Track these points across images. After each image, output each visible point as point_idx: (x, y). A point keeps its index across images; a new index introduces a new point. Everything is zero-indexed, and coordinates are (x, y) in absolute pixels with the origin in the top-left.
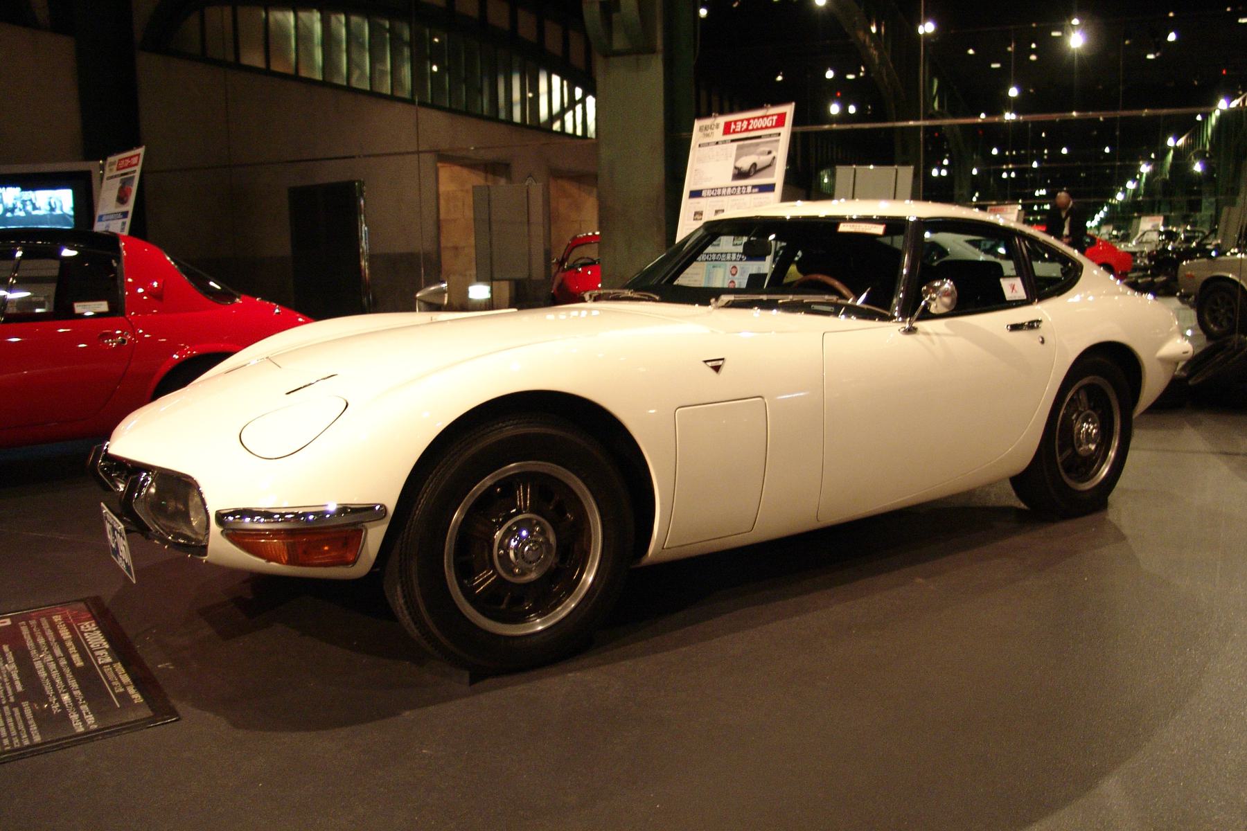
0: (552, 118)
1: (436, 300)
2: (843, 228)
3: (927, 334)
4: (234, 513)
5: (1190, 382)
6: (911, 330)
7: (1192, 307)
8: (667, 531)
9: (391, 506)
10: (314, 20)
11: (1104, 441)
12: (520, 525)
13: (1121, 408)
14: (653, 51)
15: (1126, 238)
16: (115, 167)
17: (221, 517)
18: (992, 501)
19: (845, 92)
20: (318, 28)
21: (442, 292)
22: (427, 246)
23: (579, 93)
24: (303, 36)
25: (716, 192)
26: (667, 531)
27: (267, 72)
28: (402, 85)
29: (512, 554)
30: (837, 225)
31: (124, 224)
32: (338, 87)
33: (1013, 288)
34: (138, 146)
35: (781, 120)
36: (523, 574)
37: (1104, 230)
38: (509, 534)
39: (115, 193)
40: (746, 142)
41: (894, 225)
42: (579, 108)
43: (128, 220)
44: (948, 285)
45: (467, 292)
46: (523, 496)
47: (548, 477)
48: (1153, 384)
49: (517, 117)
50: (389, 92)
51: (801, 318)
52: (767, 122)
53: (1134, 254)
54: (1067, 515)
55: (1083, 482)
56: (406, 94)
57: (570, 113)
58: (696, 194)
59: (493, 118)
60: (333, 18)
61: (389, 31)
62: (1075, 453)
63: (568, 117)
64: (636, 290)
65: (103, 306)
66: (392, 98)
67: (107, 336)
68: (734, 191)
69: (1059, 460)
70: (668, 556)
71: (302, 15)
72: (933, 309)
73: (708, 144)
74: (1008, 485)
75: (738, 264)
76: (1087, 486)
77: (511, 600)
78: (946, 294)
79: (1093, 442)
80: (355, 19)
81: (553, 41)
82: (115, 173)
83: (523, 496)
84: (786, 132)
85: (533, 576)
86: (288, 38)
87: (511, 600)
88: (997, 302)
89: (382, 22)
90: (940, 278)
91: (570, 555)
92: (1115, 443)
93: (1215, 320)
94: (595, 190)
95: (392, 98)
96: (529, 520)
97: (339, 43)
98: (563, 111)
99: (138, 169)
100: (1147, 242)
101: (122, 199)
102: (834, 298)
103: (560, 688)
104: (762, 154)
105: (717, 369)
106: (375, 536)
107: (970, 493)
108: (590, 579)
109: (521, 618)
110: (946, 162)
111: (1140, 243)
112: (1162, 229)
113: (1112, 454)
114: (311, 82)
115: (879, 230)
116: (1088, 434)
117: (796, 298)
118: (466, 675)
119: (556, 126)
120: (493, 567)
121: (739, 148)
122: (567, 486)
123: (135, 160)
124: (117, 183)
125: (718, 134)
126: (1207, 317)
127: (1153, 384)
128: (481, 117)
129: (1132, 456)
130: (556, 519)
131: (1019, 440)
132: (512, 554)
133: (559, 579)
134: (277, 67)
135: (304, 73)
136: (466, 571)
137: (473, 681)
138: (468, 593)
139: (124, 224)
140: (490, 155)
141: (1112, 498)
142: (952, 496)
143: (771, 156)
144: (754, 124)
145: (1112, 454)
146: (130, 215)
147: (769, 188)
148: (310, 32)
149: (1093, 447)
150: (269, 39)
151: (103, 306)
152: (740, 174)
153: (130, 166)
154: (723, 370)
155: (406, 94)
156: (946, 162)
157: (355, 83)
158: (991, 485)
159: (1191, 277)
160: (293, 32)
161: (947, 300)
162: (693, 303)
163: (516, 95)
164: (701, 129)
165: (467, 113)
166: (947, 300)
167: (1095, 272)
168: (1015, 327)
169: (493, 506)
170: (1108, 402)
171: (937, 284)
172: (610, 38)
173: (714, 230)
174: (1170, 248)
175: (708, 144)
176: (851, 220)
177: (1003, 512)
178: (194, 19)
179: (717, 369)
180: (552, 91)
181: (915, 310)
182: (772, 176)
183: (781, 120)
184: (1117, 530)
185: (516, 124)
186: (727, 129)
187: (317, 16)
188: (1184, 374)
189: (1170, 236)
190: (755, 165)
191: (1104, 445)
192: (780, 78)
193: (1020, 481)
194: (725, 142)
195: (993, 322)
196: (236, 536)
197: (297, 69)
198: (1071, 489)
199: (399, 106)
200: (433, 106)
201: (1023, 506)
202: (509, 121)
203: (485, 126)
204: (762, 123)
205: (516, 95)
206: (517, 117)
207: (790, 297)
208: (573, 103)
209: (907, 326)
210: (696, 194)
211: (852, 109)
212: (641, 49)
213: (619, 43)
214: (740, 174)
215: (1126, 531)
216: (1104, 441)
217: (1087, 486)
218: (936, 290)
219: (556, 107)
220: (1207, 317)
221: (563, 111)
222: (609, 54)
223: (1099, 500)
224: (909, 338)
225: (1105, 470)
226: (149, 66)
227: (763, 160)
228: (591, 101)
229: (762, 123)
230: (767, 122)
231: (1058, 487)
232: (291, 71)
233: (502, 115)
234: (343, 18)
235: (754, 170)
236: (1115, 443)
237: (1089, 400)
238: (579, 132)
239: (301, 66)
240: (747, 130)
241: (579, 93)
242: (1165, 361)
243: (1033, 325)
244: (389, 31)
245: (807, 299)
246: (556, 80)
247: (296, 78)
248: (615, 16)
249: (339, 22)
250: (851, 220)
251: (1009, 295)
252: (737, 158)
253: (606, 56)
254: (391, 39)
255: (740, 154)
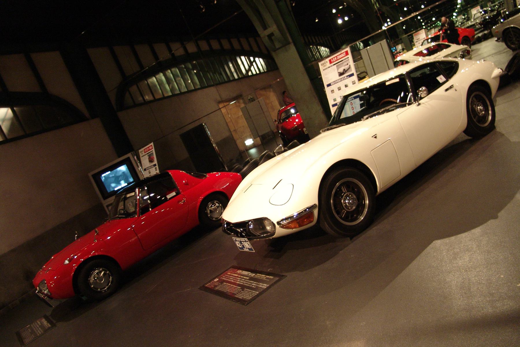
0: (247, 72)
1: (279, 151)
2: (387, 84)
3: (423, 103)
4: (282, 220)
5: (509, 74)
6: (419, 104)
7: (502, 42)
8: (381, 183)
9: (317, 203)
10: (161, 76)
11: (486, 109)
12: (347, 196)
13: (487, 97)
14: (289, 43)
15: (468, 19)
16: (143, 152)
17: (278, 223)
18: (461, 140)
19: (341, 14)
20: (163, 78)
21: (281, 147)
22: (227, 134)
23: (252, 59)
24: (160, 83)
25: (335, 82)
26: (381, 183)
27: (155, 100)
28: (196, 84)
29: (347, 204)
30: (385, 83)
31: (156, 168)
32: (178, 95)
33: (441, 79)
34: (151, 143)
35: (347, 53)
36: (351, 208)
37: (459, 18)
38: (345, 200)
39: (147, 160)
40: (338, 64)
41: (400, 76)
42: (254, 64)
43: (157, 167)
44: (424, 88)
45: (245, 144)
46: (344, 190)
47: (348, 182)
48: (494, 86)
49: (236, 77)
50: (193, 88)
51: (386, 115)
52: (343, 55)
53: (474, 25)
54: (484, 135)
55: (486, 123)
56: (199, 87)
57: (252, 67)
58: (329, 85)
59: (229, 81)
60: (167, 73)
61: (185, 68)
62: (479, 117)
63: (252, 68)
64: (337, 124)
65: (174, 194)
66: (196, 90)
67: (179, 202)
68: (341, 80)
69: (475, 120)
70: (383, 190)
71: (157, 76)
72: (422, 96)
73: (326, 69)
74: (464, 134)
75: (352, 101)
76: (487, 124)
77: (352, 215)
78: (424, 90)
79: (483, 111)
80: (173, 69)
81: (236, 46)
82: (144, 154)
83: (344, 190)
84: (350, 56)
85: (354, 208)
86: (155, 86)
87: (352, 215)
88: (439, 85)
89: (181, 66)
90: (421, 87)
91: (360, 198)
92: (490, 108)
93: (513, 43)
94: (271, 90)
95: (196, 90)
96: (347, 195)
97: (172, 80)
98: (250, 67)
99: (153, 150)
100: (477, 18)
101: (151, 161)
102: (394, 105)
103: (373, 231)
104: (345, 65)
105: (376, 137)
106: (316, 212)
107: (453, 141)
108: (368, 202)
109: (356, 219)
110: (388, 20)
111: (475, 19)
112: (481, 11)
113: (490, 112)
114: (169, 97)
115: (397, 80)
116: (480, 109)
117: (384, 109)
118: (349, 238)
119: (250, 74)
120: (344, 209)
121: (337, 66)
122: (353, 183)
123: (151, 148)
124: (147, 157)
125: (328, 64)
126: (509, 44)
127: (494, 86)
128: (225, 82)
129: (496, 109)
130: (353, 191)
131: (460, 120)
132: (347, 204)
133: (360, 206)
134: (157, 97)
135: (166, 95)
136: (338, 213)
137: (351, 239)
138: (341, 218)
139: (156, 168)
140: (235, 95)
141: (496, 124)
142: (449, 143)
143: (348, 66)
144: (339, 57)
145: (490, 112)
146: (157, 164)
147: (352, 75)
148: (162, 81)
149: (483, 112)
150: (151, 89)
151: (174, 194)
152: (341, 74)
153: (149, 150)
154: (377, 137)
155: (199, 87)
156: (388, 20)
157: (183, 91)
158: (459, 135)
159: (497, 32)
160: (157, 83)
161: (425, 92)
162: (353, 122)
163: (233, 70)
164: (322, 65)
165: (220, 84)
166: (425, 92)
167: (463, 71)
168: (447, 90)
169: (338, 195)
170: (483, 98)
171: (421, 89)
172: (274, 46)
173: (346, 98)
174: (487, 18)
175: (326, 69)
176: (388, 81)
177: (465, 142)
178: (127, 95)
179: (376, 137)
180: (243, 62)
181: (417, 98)
182: (351, 71)
183: (347, 53)
184: (500, 133)
185: (237, 79)
186: (330, 62)
187: (161, 74)
188: (506, 72)
189: (486, 12)
190: (344, 70)
191: (486, 110)
192: (317, 21)
193: (466, 131)
194: (331, 66)
195: (440, 91)
196: (283, 227)
197: (163, 95)
198: (483, 127)
199: (199, 92)
200: (209, 86)
201: (470, 138)
202: (235, 80)
203: (229, 85)
204: (341, 56)
205: (233, 70)
206: (236, 77)
207: (383, 109)
208: (251, 63)
209: (417, 104)
210: (329, 85)
211: (346, 19)
212: (285, 44)
213: (277, 45)
214: (341, 74)
215: (504, 132)
216: (486, 109)
217: (487, 124)
218: (421, 91)
219: (247, 67)
220: (509, 44)
221: (250, 67)
222: (275, 50)
223: (492, 126)
224: (420, 107)
225: (490, 118)
226: (121, 115)
227: (346, 67)
228: (257, 59)
229: (341, 56)
230: (343, 55)
231: (479, 126)
232: (162, 96)
233: (231, 79)
234: (169, 71)
235: (345, 71)
236: (490, 108)
237: (477, 99)
238: (258, 72)
239: (164, 93)
240: (337, 60)
241: (252, 59)
242: (495, 78)
243: (451, 87)
244: (185, 68)
245: (387, 108)
246: (243, 58)
247: (164, 98)
248: (273, 38)
249: (169, 73)
250: (388, 81)
251: (441, 81)
252: (338, 69)
253: (275, 51)
254: (187, 71)
255: (338, 68)
